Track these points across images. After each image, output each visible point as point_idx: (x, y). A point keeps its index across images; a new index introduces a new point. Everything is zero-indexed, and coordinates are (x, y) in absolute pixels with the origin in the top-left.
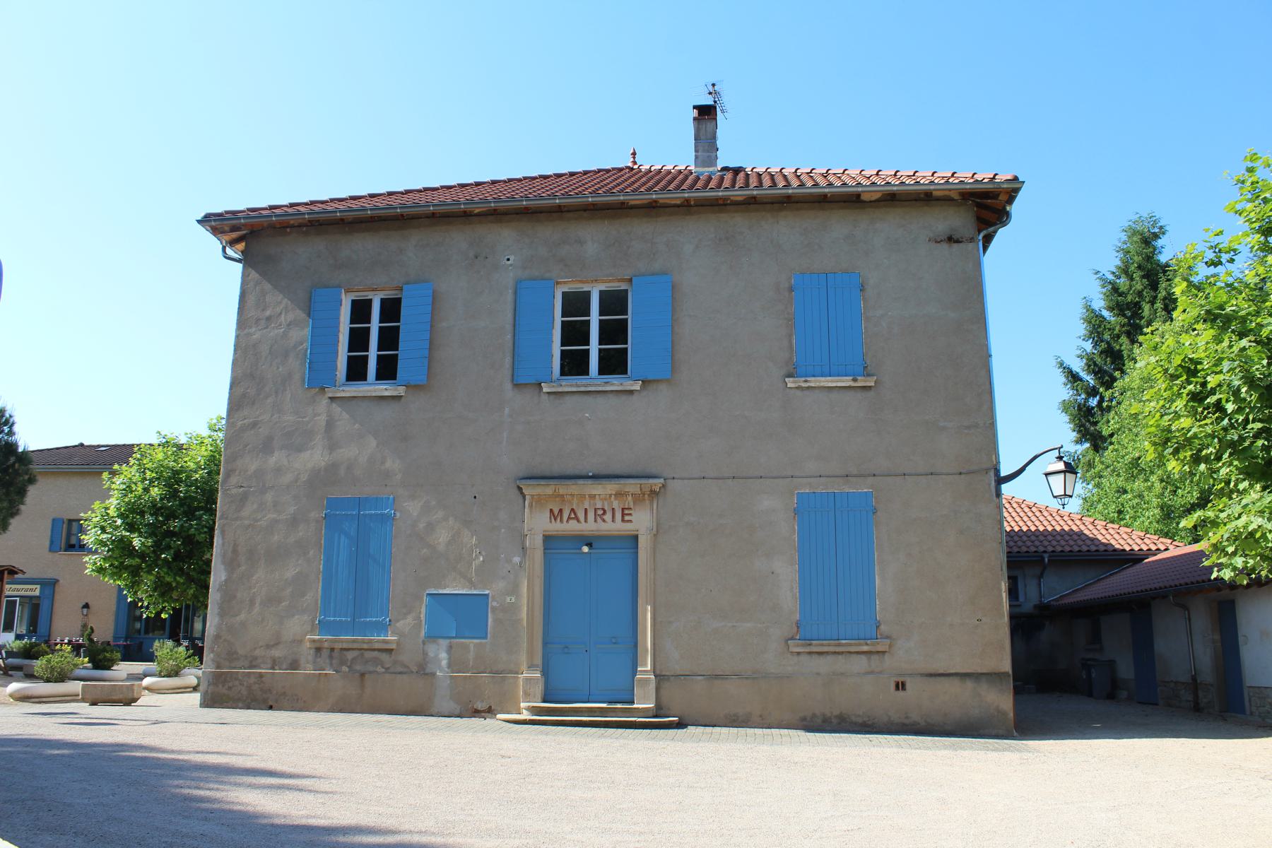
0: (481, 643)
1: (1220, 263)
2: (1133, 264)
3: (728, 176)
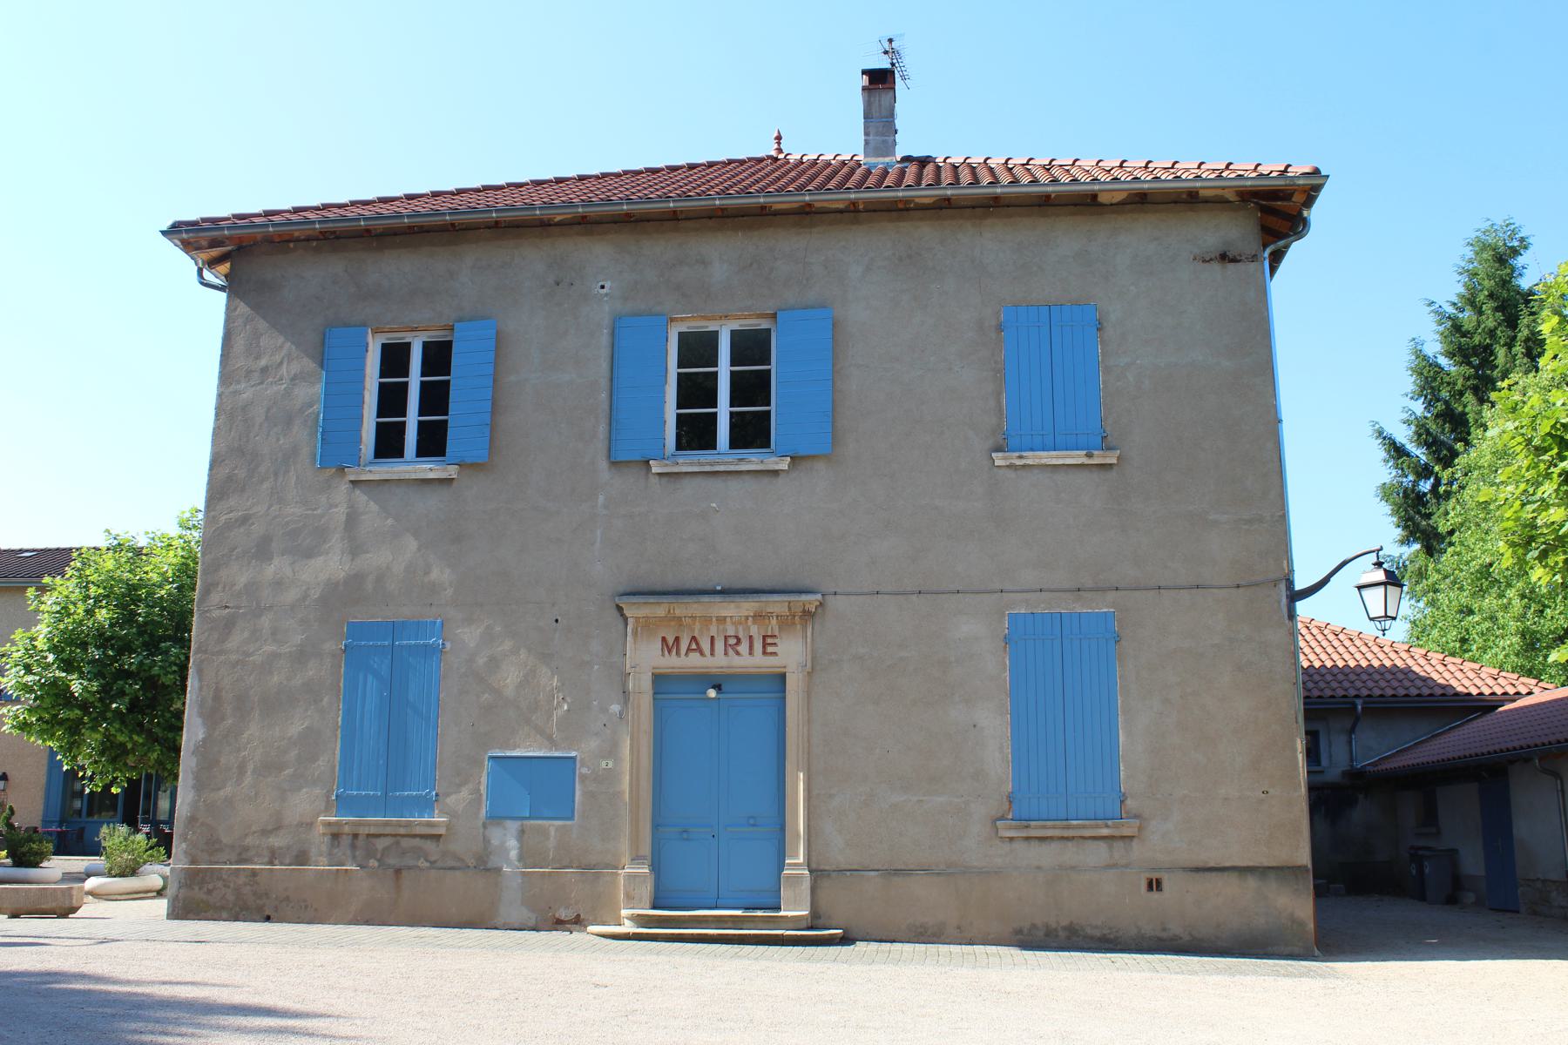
2: (1482, 290)
3: (912, 170)
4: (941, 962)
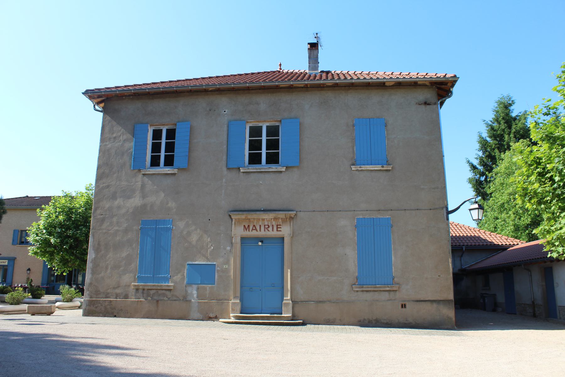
0: (212, 286)
1: (550, 114)
2: (500, 117)
3: (324, 75)
4: (335, 331)
